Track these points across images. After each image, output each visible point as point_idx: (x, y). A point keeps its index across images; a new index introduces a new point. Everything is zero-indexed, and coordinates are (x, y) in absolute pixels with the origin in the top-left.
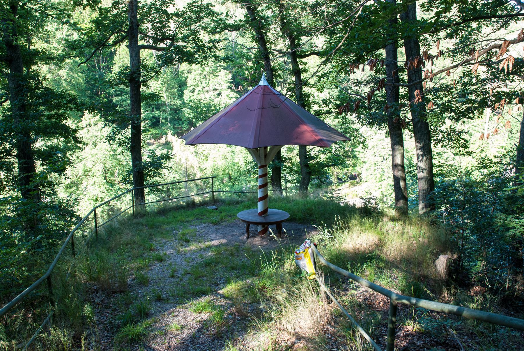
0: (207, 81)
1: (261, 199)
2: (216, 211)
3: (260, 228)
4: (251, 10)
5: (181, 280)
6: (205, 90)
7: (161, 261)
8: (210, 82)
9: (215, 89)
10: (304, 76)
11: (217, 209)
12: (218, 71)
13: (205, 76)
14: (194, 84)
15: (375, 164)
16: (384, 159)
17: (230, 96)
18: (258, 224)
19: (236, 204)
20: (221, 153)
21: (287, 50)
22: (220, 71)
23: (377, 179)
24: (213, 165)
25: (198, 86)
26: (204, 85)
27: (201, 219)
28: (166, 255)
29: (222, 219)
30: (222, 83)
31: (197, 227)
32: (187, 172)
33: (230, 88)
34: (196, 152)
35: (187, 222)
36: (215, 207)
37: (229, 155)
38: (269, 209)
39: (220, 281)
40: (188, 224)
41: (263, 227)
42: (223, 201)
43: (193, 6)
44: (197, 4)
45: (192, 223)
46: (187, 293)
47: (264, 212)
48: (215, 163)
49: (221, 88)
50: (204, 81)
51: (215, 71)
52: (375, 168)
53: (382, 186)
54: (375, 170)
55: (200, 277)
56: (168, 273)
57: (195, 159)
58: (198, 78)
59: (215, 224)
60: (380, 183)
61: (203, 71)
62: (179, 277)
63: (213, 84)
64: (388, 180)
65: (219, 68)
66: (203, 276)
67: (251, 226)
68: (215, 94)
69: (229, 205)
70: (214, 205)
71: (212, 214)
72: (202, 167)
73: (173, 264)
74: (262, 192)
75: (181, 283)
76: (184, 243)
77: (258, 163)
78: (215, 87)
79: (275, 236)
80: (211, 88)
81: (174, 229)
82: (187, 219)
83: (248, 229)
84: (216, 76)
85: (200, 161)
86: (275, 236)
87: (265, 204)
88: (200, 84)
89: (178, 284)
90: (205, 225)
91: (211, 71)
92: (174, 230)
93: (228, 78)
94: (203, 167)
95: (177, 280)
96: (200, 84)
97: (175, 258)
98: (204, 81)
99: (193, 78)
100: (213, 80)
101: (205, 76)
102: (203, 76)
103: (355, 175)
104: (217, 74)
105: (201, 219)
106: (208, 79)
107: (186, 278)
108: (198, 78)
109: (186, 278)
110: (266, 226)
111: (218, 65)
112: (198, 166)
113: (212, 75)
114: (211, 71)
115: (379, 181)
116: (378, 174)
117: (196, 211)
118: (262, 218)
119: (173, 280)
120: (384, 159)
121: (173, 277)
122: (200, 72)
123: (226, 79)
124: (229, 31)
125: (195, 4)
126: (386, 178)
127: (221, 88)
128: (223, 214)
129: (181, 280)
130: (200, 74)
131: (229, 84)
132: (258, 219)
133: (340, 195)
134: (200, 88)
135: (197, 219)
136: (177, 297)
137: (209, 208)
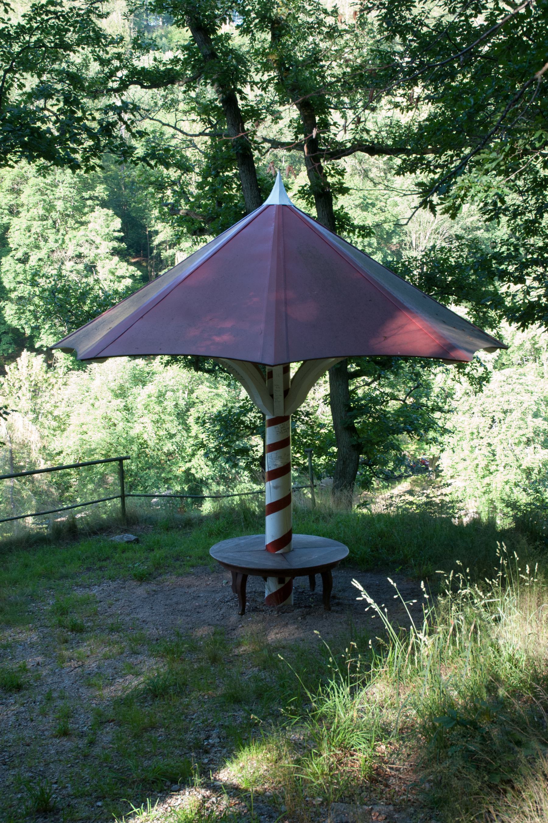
0: (60, 236)
1: (274, 507)
2: (136, 547)
3: (271, 587)
4: (203, 29)
5: (92, 743)
6: (55, 256)
7: (19, 688)
8: (67, 238)
9: (79, 256)
10: (341, 203)
11: (137, 541)
12: (86, 210)
13: (55, 222)
14: (27, 242)
15: (472, 433)
16: (493, 421)
17: (119, 273)
18: (265, 573)
19: (185, 527)
20: (99, 413)
21: (297, 138)
22: (92, 211)
23: (479, 469)
24: (78, 443)
25: (38, 247)
26: (51, 244)
27: (101, 568)
28: (24, 669)
29: (158, 566)
30: (98, 240)
31: (95, 590)
32: (12, 459)
33: (115, 252)
34: (34, 411)
35: (65, 577)
36: (132, 537)
37: (117, 417)
38: (294, 536)
39: (208, 738)
40: (67, 583)
41: (281, 581)
42: (150, 522)
43: (48, 12)
44: (59, 8)
45: (79, 580)
46: (124, 782)
47: (283, 541)
48: (85, 437)
49: (94, 251)
50: (51, 235)
51: (78, 210)
52: (472, 443)
53: (493, 486)
54: (473, 448)
55: (145, 729)
56: (49, 723)
57: (32, 427)
58: (37, 227)
59: (142, 578)
60: (487, 480)
61: (47, 210)
62: (82, 735)
63: (74, 242)
64: (506, 472)
65: (89, 202)
66: (153, 727)
67: (250, 578)
68: (81, 267)
69: (167, 530)
70: (126, 531)
71: (129, 554)
72: (51, 448)
73: (55, 695)
74: (276, 488)
75: (97, 750)
76: (70, 635)
77: (266, 411)
78: (82, 250)
79: (370, 600)
80: (71, 253)
81: (32, 598)
82: (63, 571)
83: (241, 590)
84: (82, 224)
85: (46, 432)
86: (370, 600)
87: (285, 521)
88: (42, 244)
89: (86, 756)
90: (113, 585)
91: (70, 211)
92: (33, 601)
93: (112, 228)
94: (55, 445)
95: (82, 743)
96: (42, 244)
97: (56, 679)
98: (51, 235)
99: (24, 227)
100: (75, 233)
101: (55, 222)
102: (50, 222)
103: (423, 462)
104: (84, 219)
105: (101, 568)
106: (62, 231)
107: (107, 735)
108: (37, 227)
109: (107, 735)
110: (287, 579)
111: (86, 195)
112: (40, 445)
113: (71, 222)
114: (70, 211)
115: (484, 477)
116: (480, 458)
117: (83, 547)
118: (278, 559)
119: (67, 744)
120: (493, 421)
121: (65, 733)
122: (42, 212)
123: (107, 231)
124: (143, 87)
125: (52, 9)
126: (501, 468)
127: (94, 251)
128: (158, 553)
129: (92, 743)
130: (43, 218)
131: (116, 244)
132: (270, 562)
133: (447, 499)
134: (43, 254)
135: (88, 569)
136: (98, 798)
137: (117, 538)
